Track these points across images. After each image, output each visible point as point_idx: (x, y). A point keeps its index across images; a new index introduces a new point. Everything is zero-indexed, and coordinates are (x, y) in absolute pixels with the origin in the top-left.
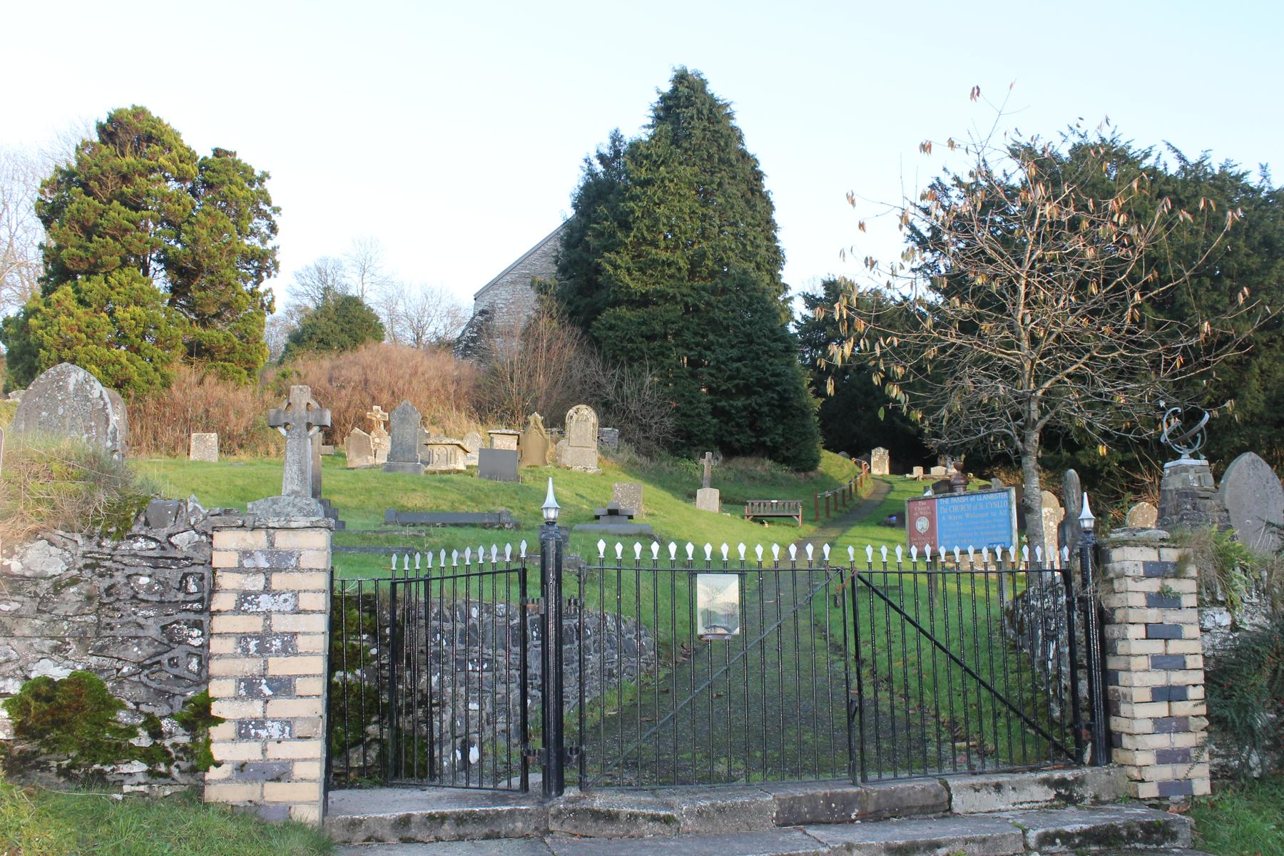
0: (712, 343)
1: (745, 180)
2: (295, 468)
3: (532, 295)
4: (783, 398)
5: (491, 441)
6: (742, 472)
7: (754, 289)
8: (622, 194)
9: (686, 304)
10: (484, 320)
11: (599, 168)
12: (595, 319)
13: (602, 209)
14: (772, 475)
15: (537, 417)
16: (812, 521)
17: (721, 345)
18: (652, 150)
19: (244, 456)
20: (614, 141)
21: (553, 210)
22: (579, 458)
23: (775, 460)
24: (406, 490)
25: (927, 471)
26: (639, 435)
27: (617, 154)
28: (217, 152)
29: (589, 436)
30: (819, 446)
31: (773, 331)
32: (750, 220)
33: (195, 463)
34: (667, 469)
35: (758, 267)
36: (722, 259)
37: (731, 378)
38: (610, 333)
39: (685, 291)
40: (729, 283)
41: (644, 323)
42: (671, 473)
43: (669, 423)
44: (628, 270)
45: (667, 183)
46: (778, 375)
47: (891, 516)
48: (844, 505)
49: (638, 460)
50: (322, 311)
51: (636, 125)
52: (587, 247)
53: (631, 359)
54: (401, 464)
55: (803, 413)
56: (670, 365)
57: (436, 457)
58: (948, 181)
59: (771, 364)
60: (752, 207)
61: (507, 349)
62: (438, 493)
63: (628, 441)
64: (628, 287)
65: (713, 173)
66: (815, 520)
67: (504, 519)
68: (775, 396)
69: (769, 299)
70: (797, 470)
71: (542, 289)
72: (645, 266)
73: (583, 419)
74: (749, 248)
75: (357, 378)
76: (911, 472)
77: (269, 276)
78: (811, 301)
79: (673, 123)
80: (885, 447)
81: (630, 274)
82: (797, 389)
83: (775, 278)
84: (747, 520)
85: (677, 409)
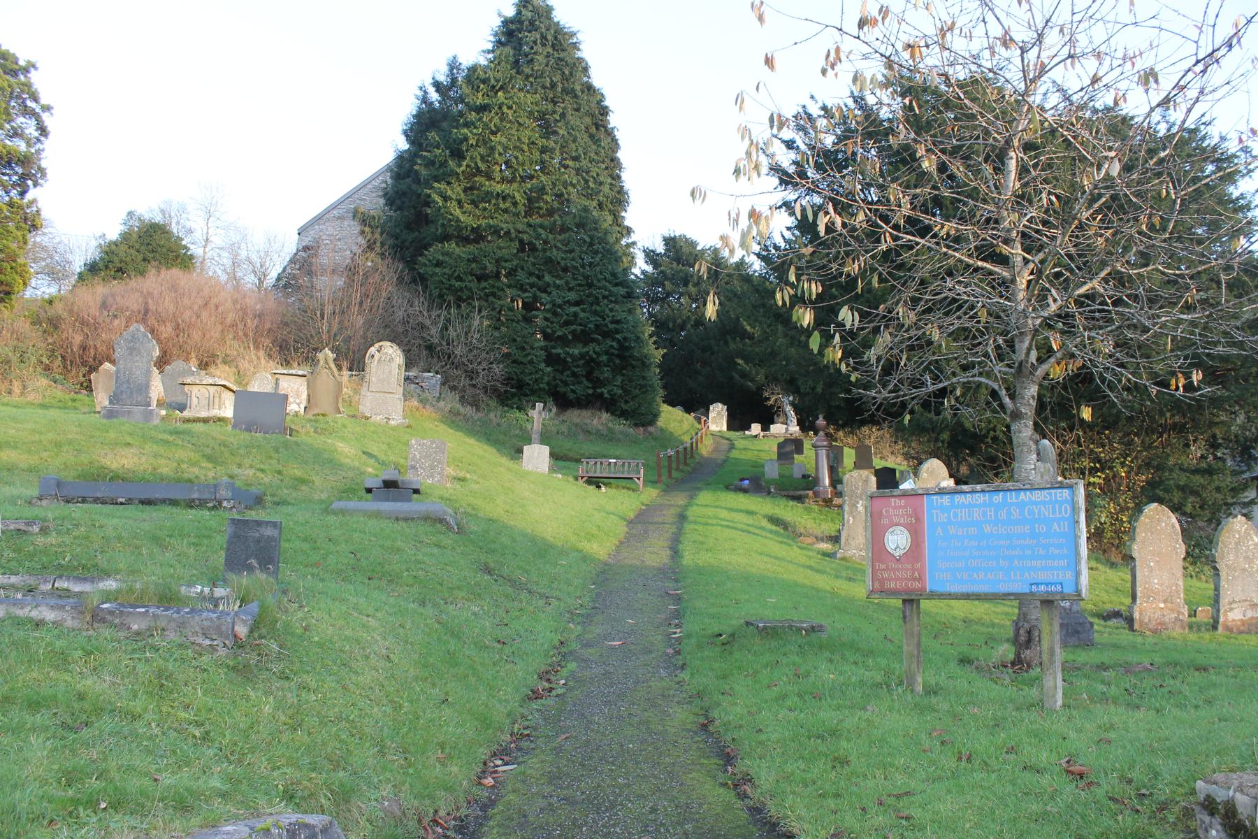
0: (548, 285)
1: (588, 113)
3: (355, 227)
4: (623, 348)
5: (277, 384)
6: (576, 425)
7: (596, 229)
8: (457, 120)
9: (521, 242)
10: (305, 260)
11: (434, 96)
12: (421, 255)
13: (433, 135)
14: (609, 429)
15: (327, 354)
16: (654, 483)
17: (558, 287)
18: (490, 74)
20: (451, 69)
22: (383, 404)
23: (612, 414)
24: (114, 444)
25: (765, 428)
26: (465, 382)
29: (394, 380)
30: (659, 399)
31: (614, 274)
32: (592, 155)
34: (495, 421)
35: (600, 205)
36: (562, 195)
37: (567, 323)
38: (437, 270)
39: (520, 227)
40: (569, 220)
41: (474, 260)
42: (499, 425)
43: (498, 369)
44: (459, 202)
45: (505, 109)
46: (618, 322)
47: (742, 480)
48: (686, 464)
49: (462, 410)
51: (474, 46)
52: (417, 180)
53: (459, 300)
54: (126, 408)
55: (643, 363)
56: (502, 306)
57: (195, 400)
58: (815, 111)
59: (611, 310)
60: (597, 142)
61: (328, 285)
62: (161, 450)
63: (453, 388)
64: (458, 220)
65: (555, 103)
66: (656, 482)
67: (223, 493)
69: (612, 240)
70: (636, 425)
71: (365, 221)
72: (477, 197)
73: (387, 359)
74: (591, 185)
75: (135, 307)
76: (749, 428)
78: (651, 256)
79: (515, 49)
80: (724, 404)
81: (461, 207)
82: (638, 338)
83: (617, 220)
84: (581, 482)
85: (507, 355)
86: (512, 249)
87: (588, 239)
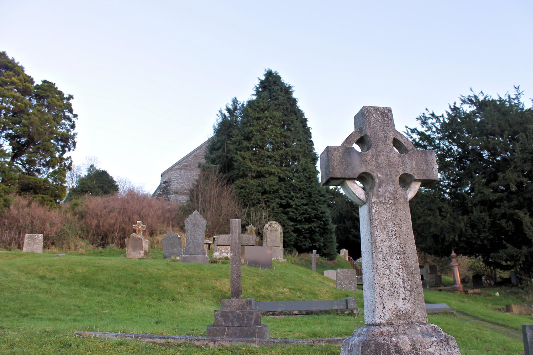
0: (293, 197)
2: (395, 264)
9: (279, 177)
17: (297, 198)
19: (54, 249)
21: (205, 132)
27: (235, 109)
28: (45, 82)
29: (278, 240)
33: (27, 254)
38: (242, 190)
41: (259, 186)
50: (89, 177)
51: (247, 94)
54: (193, 256)
58: (427, 115)
68: (322, 223)
70: (330, 260)
77: (69, 150)
80: (346, 249)
81: (251, 162)
86: (275, 180)
87: (308, 176)
